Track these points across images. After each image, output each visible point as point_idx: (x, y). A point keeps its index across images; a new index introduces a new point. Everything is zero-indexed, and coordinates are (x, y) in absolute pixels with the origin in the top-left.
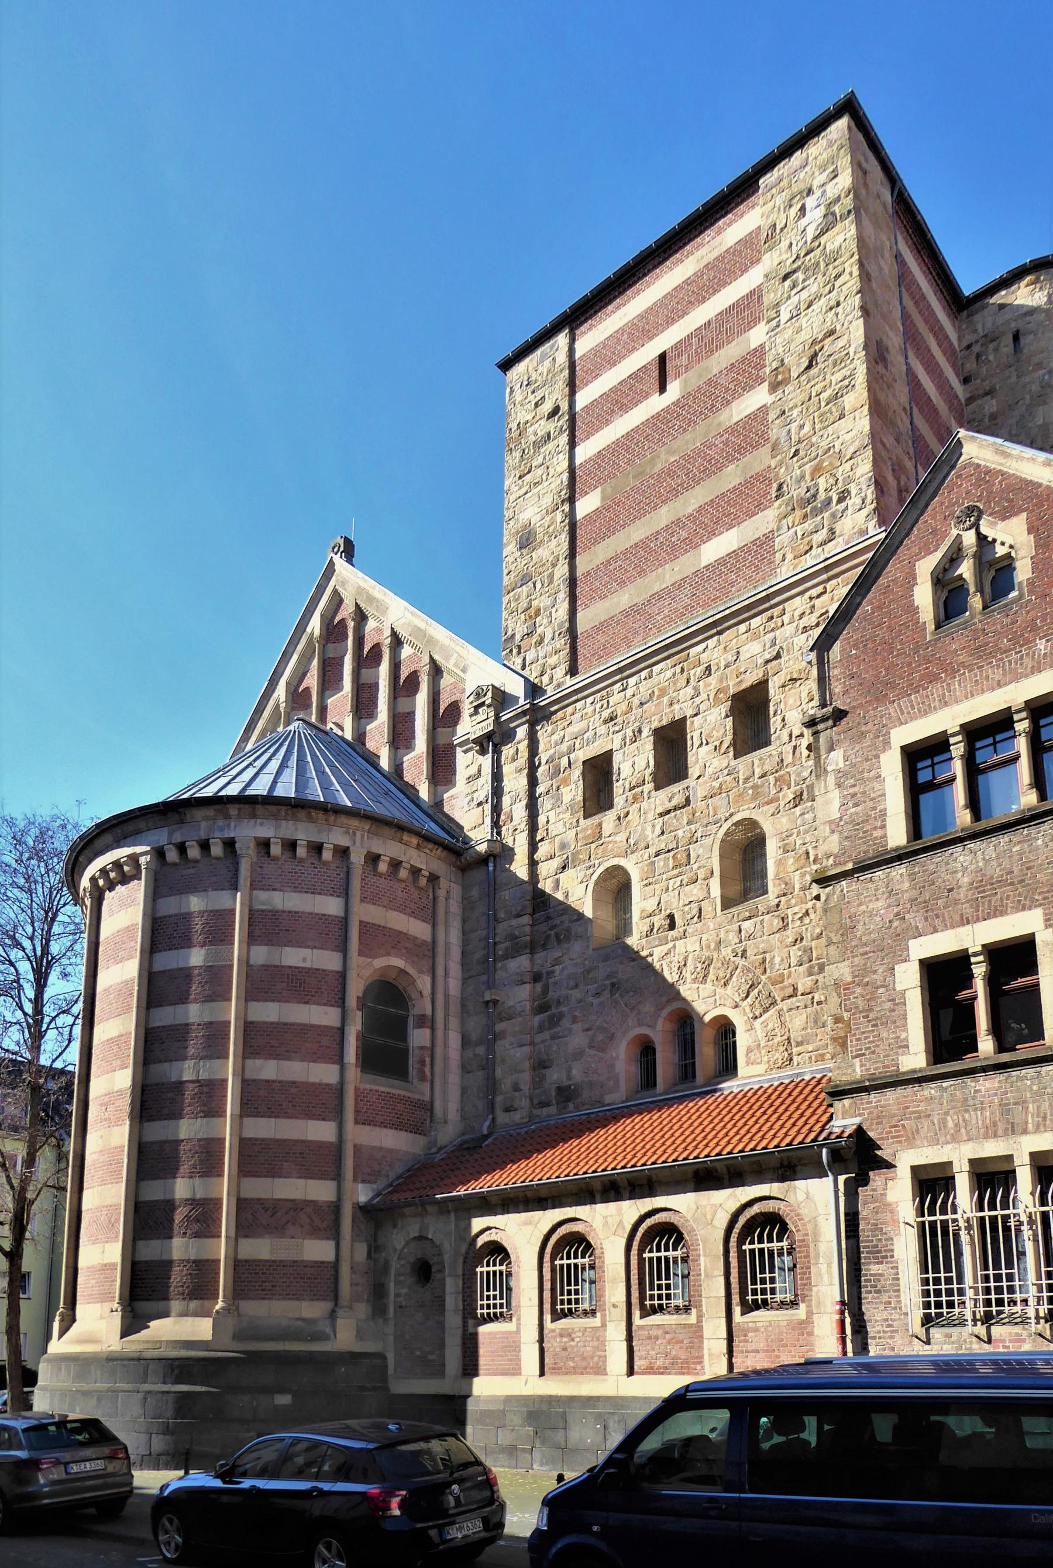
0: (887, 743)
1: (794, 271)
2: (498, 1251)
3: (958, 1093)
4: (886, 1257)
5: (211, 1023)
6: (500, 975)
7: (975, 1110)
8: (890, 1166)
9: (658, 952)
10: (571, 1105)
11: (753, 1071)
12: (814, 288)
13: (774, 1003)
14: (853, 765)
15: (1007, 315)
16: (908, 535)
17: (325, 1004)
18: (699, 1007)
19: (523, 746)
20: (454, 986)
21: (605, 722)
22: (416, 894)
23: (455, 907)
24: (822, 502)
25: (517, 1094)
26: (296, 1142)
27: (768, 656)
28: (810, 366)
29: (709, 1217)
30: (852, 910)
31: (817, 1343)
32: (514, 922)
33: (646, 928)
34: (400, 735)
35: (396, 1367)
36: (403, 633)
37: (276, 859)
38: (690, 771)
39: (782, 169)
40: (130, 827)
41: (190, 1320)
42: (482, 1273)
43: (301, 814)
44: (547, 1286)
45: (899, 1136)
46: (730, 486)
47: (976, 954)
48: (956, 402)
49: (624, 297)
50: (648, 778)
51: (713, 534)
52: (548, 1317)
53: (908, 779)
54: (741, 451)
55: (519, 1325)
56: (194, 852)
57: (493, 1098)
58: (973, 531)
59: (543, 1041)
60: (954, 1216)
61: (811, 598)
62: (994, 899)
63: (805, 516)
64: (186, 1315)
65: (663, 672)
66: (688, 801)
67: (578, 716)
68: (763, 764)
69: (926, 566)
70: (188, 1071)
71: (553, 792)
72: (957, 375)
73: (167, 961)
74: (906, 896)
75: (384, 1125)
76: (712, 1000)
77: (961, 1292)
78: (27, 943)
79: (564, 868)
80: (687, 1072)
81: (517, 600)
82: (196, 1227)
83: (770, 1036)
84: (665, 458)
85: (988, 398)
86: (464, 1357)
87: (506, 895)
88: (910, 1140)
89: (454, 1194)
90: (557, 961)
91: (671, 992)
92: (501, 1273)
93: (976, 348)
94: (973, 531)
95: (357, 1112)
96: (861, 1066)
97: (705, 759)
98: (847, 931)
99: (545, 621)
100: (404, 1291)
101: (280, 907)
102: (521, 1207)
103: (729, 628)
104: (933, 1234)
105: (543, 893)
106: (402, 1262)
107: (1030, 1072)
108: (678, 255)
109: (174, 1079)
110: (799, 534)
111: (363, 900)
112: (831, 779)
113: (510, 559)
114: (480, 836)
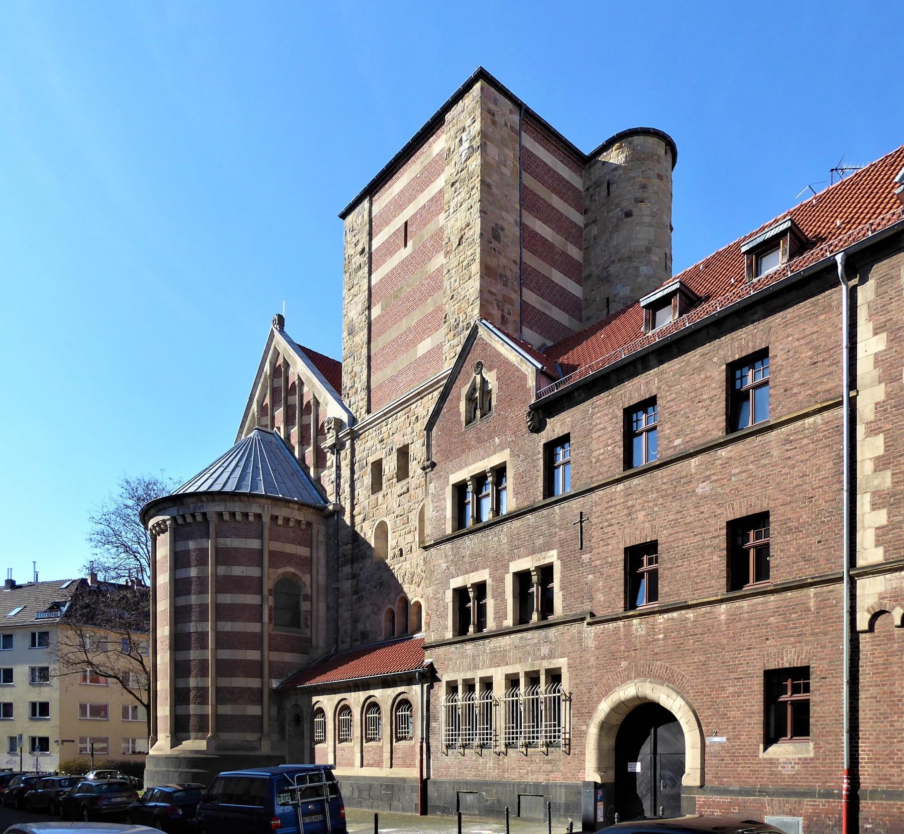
0: (448, 481)
2: (321, 711)
6: (340, 574)
9: (397, 567)
18: (410, 596)
20: (322, 579)
23: (322, 538)
26: (241, 660)
28: (459, 245)
37: (227, 521)
40: (161, 506)
41: (198, 741)
43: (236, 499)
51: (423, 339)
56: (189, 519)
66: (408, 489)
69: (465, 390)
70: (192, 627)
82: (199, 700)
87: (342, 533)
88: (446, 670)
91: (399, 588)
93: (591, 191)
101: (230, 546)
107: (481, 642)
111: (270, 539)
113: (345, 340)
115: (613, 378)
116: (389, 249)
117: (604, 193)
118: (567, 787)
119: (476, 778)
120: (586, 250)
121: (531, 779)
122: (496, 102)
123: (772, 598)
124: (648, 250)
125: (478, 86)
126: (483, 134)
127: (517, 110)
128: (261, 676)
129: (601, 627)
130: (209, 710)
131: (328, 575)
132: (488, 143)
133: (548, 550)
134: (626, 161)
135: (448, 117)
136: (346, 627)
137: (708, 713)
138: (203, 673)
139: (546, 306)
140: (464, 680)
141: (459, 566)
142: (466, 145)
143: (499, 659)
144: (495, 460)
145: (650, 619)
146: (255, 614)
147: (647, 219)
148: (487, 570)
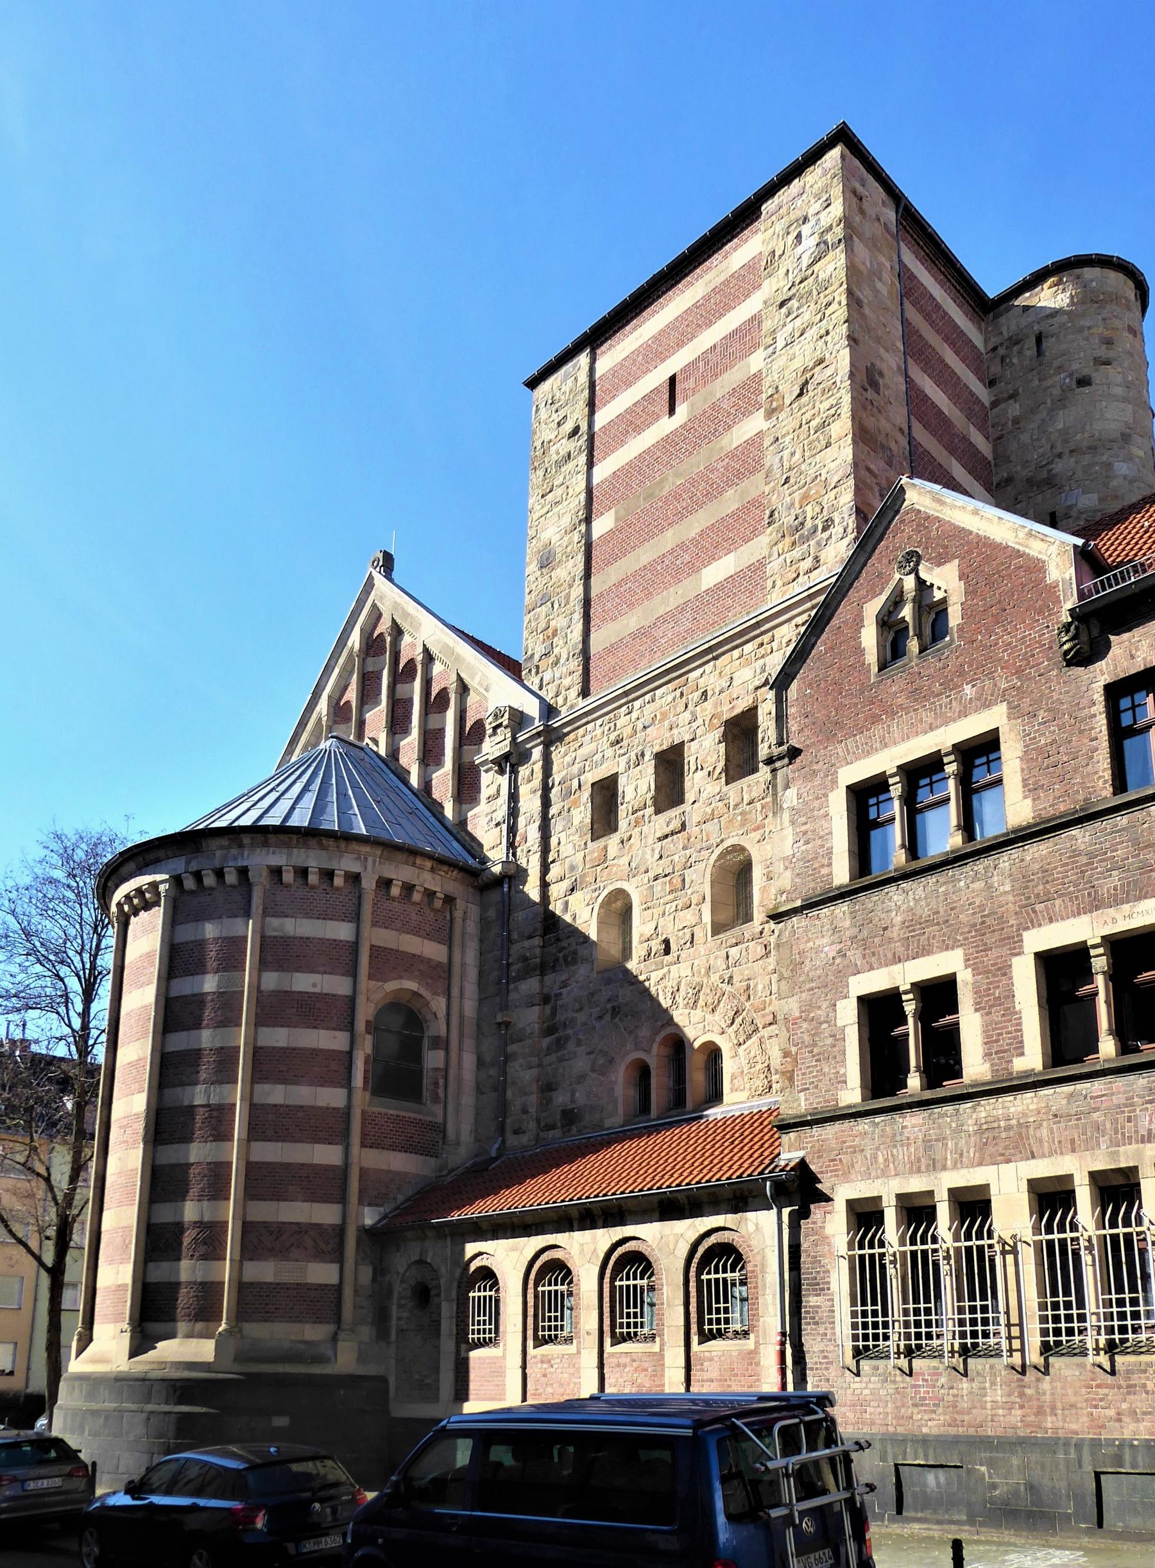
0: (835, 782)
1: (790, 299)
2: (488, 1275)
3: (888, 1128)
4: (823, 1289)
5: (222, 1048)
6: (513, 996)
7: (902, 1145)
8: (828, 1199)
9: (655, 976)
10: (574, 1129)
11: (738, 1098)
12: (806, 316)
13: (756, 1030)
14: (806, 803)
15: (1030, 317)
16: (857, 577)
17: (334, 1029)
18: (690, 1033)
19: (538, 767)
20: (470, 1007)
21: (612, 745)
22: (430, 916)
23: (472, 927)
24: (809, 530)
25: (525, 1116)
26: (303, 1166)
27: (758, 683)
28: (801, 395)
29: (671, 1247)
30: (801, 947)
31: (763, 1374)
32: (527, 943)
33: (644, 953)
34: (430, 754)
35: (397, 1389)
36: (434, 650)
37: (288, 886)
38: (687, 796)
39: (783, 196)
40: (151, 856)
41: (194, 1341)
42: (474, 1298)
43: (313, 842)
44: (531, 1312)
45: (836, 1170)
46: (729, 511)
47: (906, 992)
48: (977, 408)
49: (640, 319)
50: (649, 802)
51: (714, 558)
52: (530, 1343)
53: (854, 818)
54: (740, 475)
55: (505, 1350)
56: (209, 880)
57: (504, 1121)
58: (913, 576)
59: (550, 1064)
60: (990, 1242)
61: (797, 626)
62: (922, 938)
63: (794, 543)
64: (192, 1337)
65: (665, 695)
66: (683, 826)
67: (588, 737)
68: (751, 791)
69: (873, 608)
70: (199, 1095)
71: (564, 814)
72: (981, 379)
73: (183, 987)
74: (848, 933)
75: (393, 1148)
76: (701, 1026)
77: (1082, 1318)
78: (77, 959)
79: (572, 890)
80: (678, 1099)
81: (537, 619)
82: (202, 1250)
83: (752, 1063)
84: (673, 481)
85: (1012, 401)
86: (456, 1381)
87: (519, 916)
88: (846, 1176)
89: (449, 1219)
90: (564, 984)
91: (664, 1018)
92: (642, 1288)
93: (1001, 351)
94: (913, 576)
95: (364, 1135)
96: (806, 1100)
97: (700, 784)
98: (796, 966)
99: (561, 642)
100: (405, 1315)
101: (292, 934)
102: (509, 1233)
103: (723, 653)
104: (1063, 1252)
105: (553, 914)
106: (405, 1286)
107: (949, 1109)
108: (688, 278)
109: (186, 1103)
110: (788, 561)
111: (374, 924)
112: (786, 816)
113: (532, 578)
114: (496, 855)
116: (633, 422)
119: (952, 1431)
120: (997, 441)
124: (1126, 438)
125: (835, 153)
128: (343, 1200)
130: (226, 1271)
131: (481, 1000)
133: (1139, 898)
134: (1072, 303)
135: (768, 207)
140: (899, 1197)
141: (873, 947)
146: (337, 1069)
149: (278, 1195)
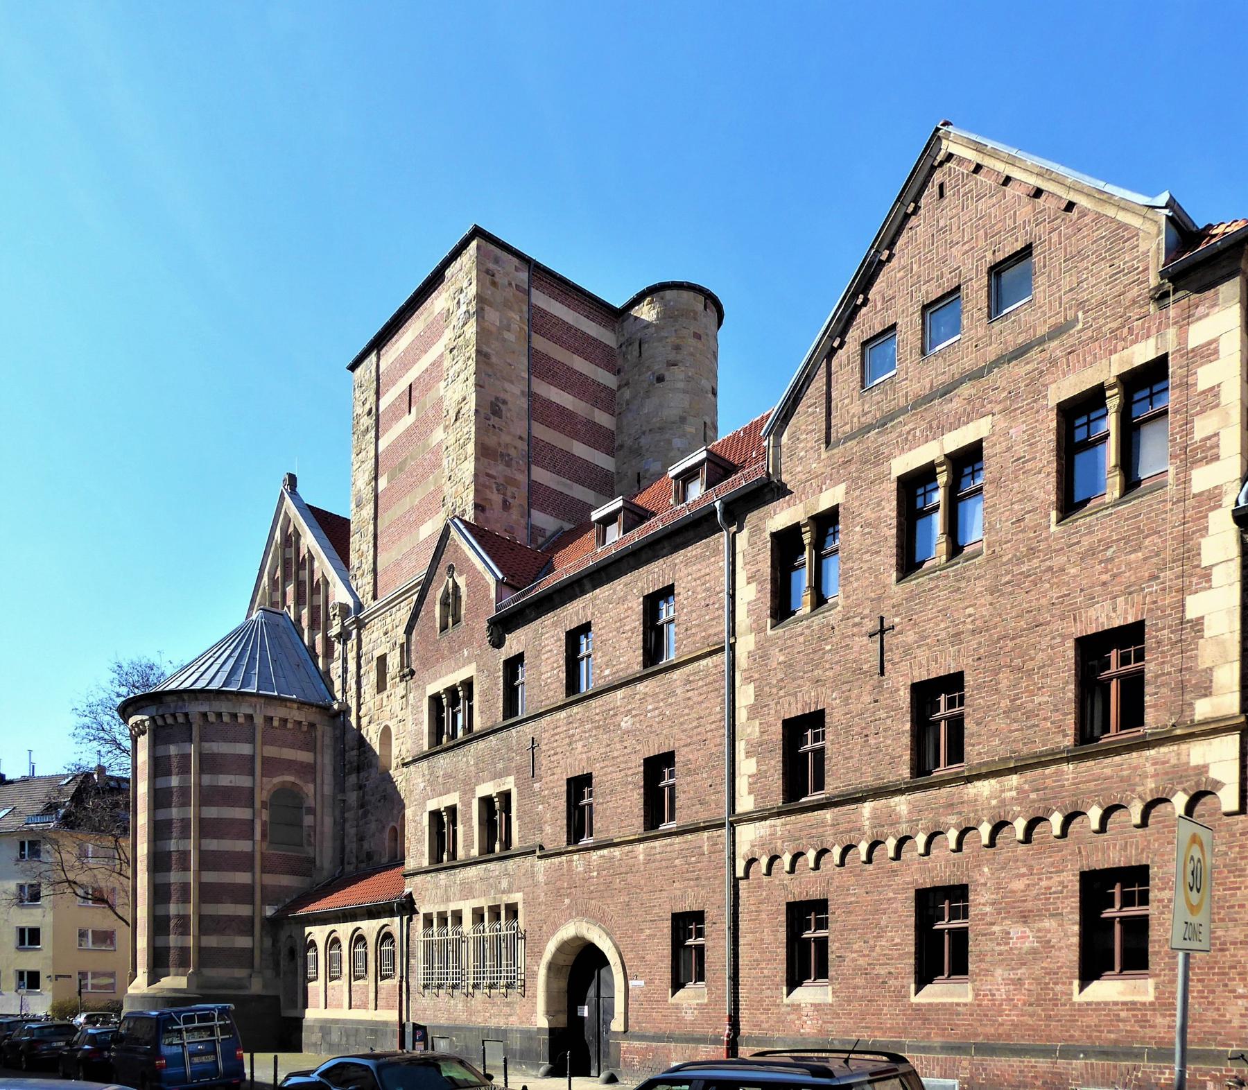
2: (313, 944)
20: (328, 789)
23: (327, 741)
43: (223, 697)
56: (170, 721)
70: (173, 845)
75: (282, 873)
87: (349, 736)
93: (624, 348)
115: (557, 599)
117: (636, 353)
118: (522, 1031)
121: (493, 1023)
122: (497, 261)
123: (678, 839)
124: (683, 420)
125: (474, 244)
126: (480, 298)
127: (525, 267)
128: (252, 903)
129: (548, 861)
130: (191, 942)
132: (487, 308)
134: (658, 318)
135: (448, 273)
136: (351, 846)
137: (631, 955)
138: (185, 899)
139: (564, 484)
142: (463, 308)
143: (467, 891)
144: (455, 678)
145: (587, 855)
146: (246, 830)
147: (681, 385)
148: (457, 794)
149: (217, 900)
